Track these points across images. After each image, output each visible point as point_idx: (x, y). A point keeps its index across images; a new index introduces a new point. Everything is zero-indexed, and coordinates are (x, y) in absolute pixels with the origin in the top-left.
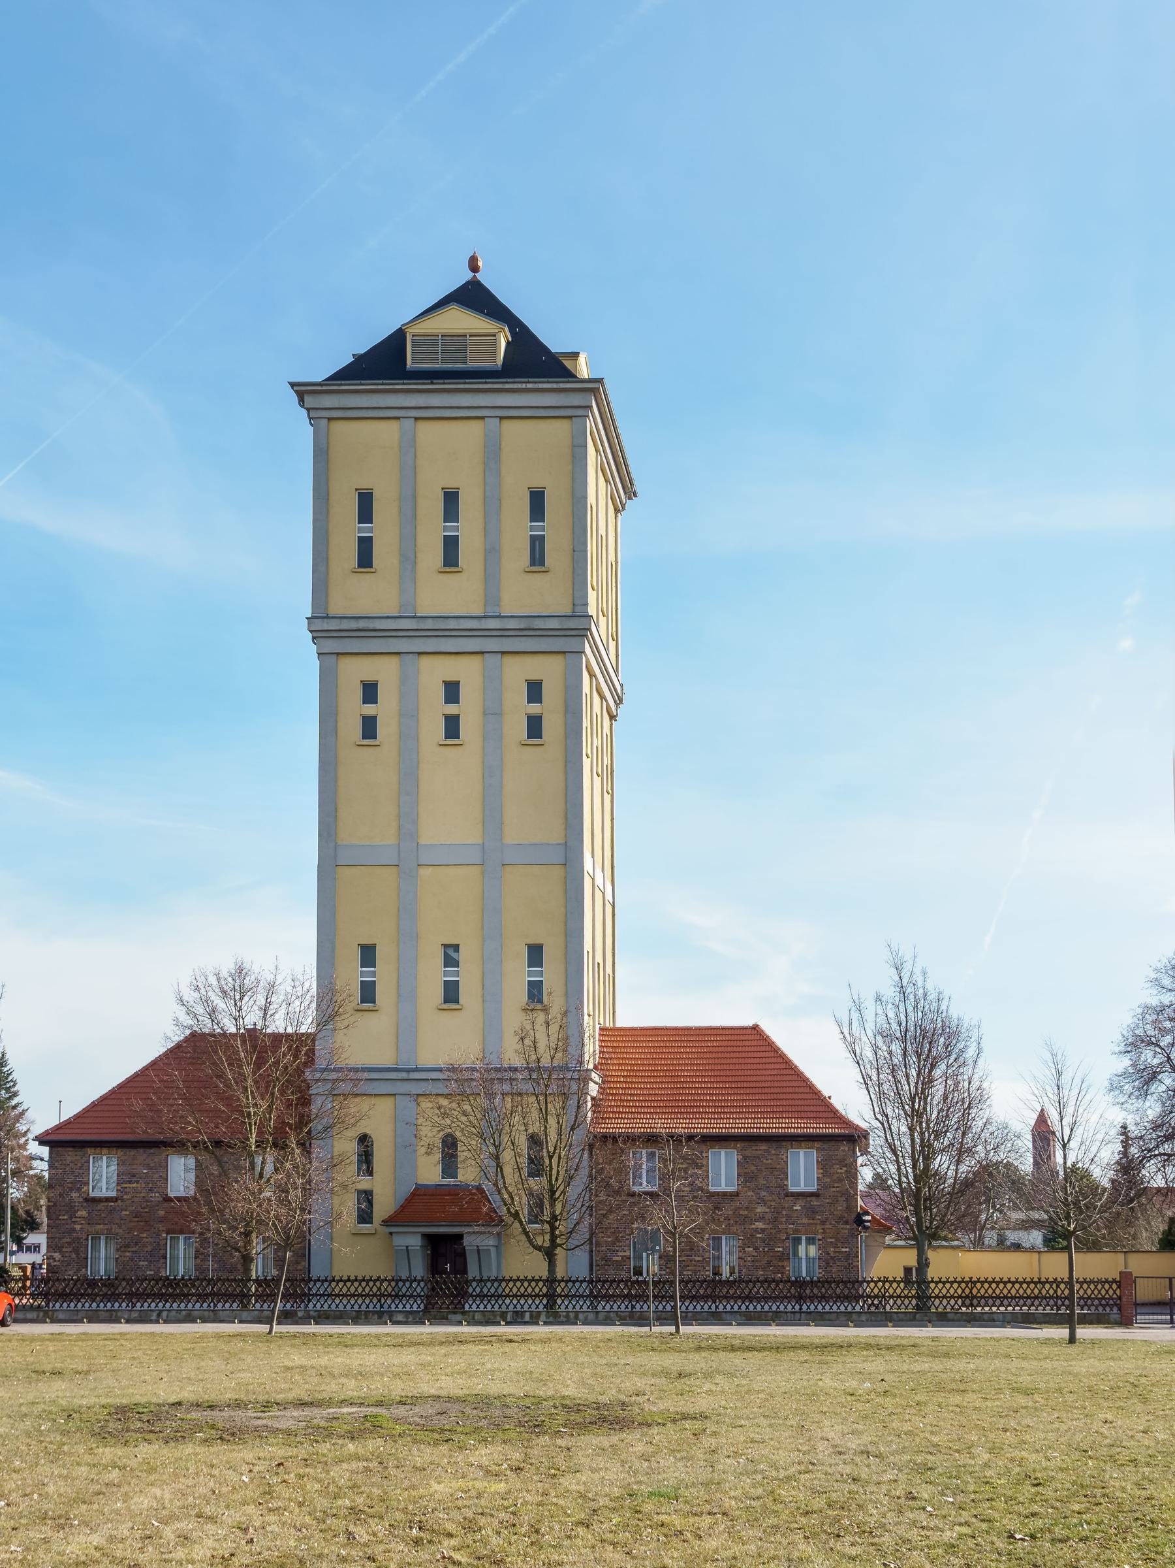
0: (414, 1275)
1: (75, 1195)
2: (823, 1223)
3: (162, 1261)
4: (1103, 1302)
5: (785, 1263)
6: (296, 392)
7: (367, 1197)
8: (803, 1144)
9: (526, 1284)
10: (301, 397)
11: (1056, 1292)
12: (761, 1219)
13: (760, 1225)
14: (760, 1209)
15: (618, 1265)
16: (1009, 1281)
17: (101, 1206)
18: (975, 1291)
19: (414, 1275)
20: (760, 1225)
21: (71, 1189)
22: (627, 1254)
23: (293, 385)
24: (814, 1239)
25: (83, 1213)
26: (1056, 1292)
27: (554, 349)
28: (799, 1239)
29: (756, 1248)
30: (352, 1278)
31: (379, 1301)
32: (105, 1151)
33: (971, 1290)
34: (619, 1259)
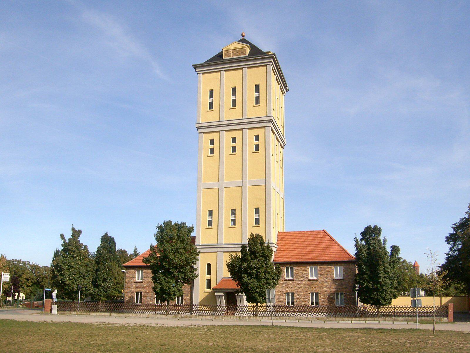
0: (435, 305)
1: (132, 281)
2: (346, 288)
3: (154, 299)
4: (98, 309)
5: (334, 301)
6: (194, 67)
7: (209, 282)
8: (338, 264)
9: (430, 308)
10: (195, 68)
11: (424, 310)
12: (326, 287)
13: (325, 289)
14: (325, 284)
15: (282, 301)
16: (427, 307)
17: (139, 284)
18: (395, 310)
19: (435, 305)
20: (325, 289)
21: (131, 279)
22: (285, 298)
23: (193, 66)
24: (343, 293)
25: (134, 286)
26: (424, 310)
27: (264, 51)
28: (338, 293)
29: (324, 296)
30: (395, 306)
31: (203, 312)
32: (140, 269)
33: (394, 310)
34: (282, 299)
